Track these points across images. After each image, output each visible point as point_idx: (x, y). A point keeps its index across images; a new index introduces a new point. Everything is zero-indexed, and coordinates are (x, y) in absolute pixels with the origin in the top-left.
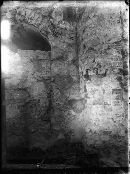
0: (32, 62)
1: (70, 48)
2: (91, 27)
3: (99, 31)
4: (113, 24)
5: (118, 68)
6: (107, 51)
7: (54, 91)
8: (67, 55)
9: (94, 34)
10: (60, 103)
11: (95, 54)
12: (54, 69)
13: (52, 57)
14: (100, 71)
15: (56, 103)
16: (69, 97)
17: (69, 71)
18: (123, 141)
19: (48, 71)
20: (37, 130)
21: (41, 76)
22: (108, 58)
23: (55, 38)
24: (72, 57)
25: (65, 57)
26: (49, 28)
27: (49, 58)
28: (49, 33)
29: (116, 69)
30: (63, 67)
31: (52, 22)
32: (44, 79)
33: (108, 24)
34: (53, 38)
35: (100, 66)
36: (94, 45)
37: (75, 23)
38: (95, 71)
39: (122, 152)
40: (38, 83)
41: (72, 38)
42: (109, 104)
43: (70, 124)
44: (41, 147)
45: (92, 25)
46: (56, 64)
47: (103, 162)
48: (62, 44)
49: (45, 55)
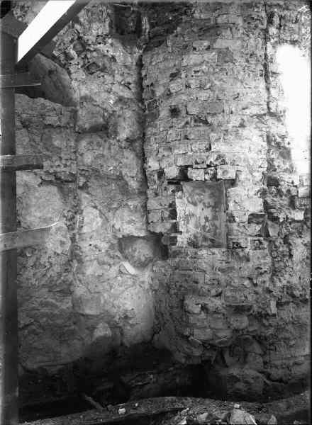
0: (24, 127)
1: (122, 108)
2: (198, 71)
3: (221, 85)
4: (251, 75)
5: (260, 169)
6: (240, 130)
7: (84, 214)
8: (115, 125)
9: (210, 88)
10: (99, 244)
11: (212, 134)
12: (86, 154)
13: (80, 123)
14: (223, 173)
15: (90, 245)
16: (119, 230)
17: (121, 165)
18: (273, 324)
19: (71, 159)
20: (35, 321)
21: (52, 171)
22: (241, 147)
23: (87, 75)
24: (127, 131)
25: (111, 128)
26: (72, 46)
27: (72, 125)
28: (72, 59)
29: (258, 171)
30: (106, 152)
31: (79, 33)
32: (58, 178)
33: (242, 73)
34: (82, 75)
35: (224, 162)
36: (208, 112)
37: (137, 50)
38: (209, 171)
39: (272, 347)
40: (42, 188)
41: (127, 85)
42: (243, 245)
43: (125, 298)
44: (46, 366)
45: (204, 67)
46: (90, 143)
47: (235, 377)
48: (104, 95)
49: (64, 115)
